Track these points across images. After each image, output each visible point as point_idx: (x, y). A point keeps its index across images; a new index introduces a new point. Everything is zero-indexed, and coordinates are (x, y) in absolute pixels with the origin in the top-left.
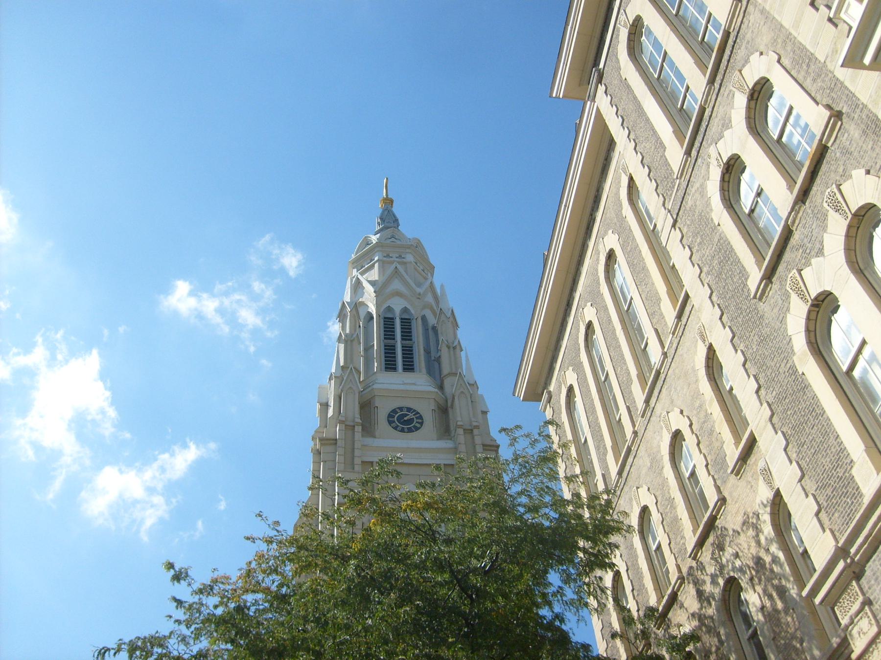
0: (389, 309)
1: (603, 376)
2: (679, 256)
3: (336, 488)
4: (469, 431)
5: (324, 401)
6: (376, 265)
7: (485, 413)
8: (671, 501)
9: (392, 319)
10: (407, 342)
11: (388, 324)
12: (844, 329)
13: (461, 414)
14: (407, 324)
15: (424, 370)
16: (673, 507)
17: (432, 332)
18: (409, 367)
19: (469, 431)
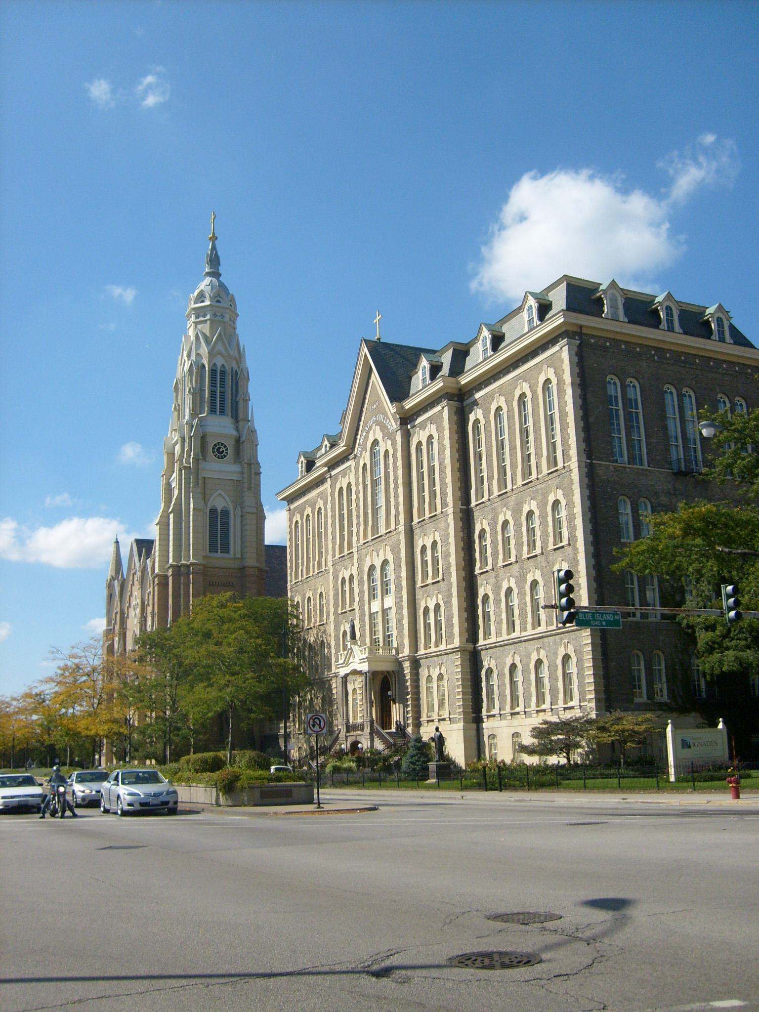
0: (215, 364)
1: (365, 354)
2: (397, 691)
3: (191, 499)
4: (250, 464)
5: (183, 436)
6: (208, 322)
7: (257, 445)
8: (525, 603)
9: (215, 370)
10: (223, 389)
11: (213, 372)
12: (385, 607)
13: (246, 449)
14: (223, 373)
15: (230, 414)
16: (556, 671)
17: (235, 374)
18: (222, 412)
19: (250, 464)
